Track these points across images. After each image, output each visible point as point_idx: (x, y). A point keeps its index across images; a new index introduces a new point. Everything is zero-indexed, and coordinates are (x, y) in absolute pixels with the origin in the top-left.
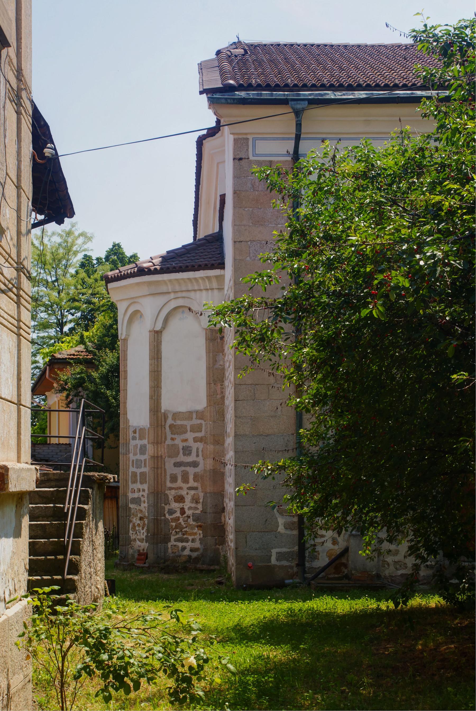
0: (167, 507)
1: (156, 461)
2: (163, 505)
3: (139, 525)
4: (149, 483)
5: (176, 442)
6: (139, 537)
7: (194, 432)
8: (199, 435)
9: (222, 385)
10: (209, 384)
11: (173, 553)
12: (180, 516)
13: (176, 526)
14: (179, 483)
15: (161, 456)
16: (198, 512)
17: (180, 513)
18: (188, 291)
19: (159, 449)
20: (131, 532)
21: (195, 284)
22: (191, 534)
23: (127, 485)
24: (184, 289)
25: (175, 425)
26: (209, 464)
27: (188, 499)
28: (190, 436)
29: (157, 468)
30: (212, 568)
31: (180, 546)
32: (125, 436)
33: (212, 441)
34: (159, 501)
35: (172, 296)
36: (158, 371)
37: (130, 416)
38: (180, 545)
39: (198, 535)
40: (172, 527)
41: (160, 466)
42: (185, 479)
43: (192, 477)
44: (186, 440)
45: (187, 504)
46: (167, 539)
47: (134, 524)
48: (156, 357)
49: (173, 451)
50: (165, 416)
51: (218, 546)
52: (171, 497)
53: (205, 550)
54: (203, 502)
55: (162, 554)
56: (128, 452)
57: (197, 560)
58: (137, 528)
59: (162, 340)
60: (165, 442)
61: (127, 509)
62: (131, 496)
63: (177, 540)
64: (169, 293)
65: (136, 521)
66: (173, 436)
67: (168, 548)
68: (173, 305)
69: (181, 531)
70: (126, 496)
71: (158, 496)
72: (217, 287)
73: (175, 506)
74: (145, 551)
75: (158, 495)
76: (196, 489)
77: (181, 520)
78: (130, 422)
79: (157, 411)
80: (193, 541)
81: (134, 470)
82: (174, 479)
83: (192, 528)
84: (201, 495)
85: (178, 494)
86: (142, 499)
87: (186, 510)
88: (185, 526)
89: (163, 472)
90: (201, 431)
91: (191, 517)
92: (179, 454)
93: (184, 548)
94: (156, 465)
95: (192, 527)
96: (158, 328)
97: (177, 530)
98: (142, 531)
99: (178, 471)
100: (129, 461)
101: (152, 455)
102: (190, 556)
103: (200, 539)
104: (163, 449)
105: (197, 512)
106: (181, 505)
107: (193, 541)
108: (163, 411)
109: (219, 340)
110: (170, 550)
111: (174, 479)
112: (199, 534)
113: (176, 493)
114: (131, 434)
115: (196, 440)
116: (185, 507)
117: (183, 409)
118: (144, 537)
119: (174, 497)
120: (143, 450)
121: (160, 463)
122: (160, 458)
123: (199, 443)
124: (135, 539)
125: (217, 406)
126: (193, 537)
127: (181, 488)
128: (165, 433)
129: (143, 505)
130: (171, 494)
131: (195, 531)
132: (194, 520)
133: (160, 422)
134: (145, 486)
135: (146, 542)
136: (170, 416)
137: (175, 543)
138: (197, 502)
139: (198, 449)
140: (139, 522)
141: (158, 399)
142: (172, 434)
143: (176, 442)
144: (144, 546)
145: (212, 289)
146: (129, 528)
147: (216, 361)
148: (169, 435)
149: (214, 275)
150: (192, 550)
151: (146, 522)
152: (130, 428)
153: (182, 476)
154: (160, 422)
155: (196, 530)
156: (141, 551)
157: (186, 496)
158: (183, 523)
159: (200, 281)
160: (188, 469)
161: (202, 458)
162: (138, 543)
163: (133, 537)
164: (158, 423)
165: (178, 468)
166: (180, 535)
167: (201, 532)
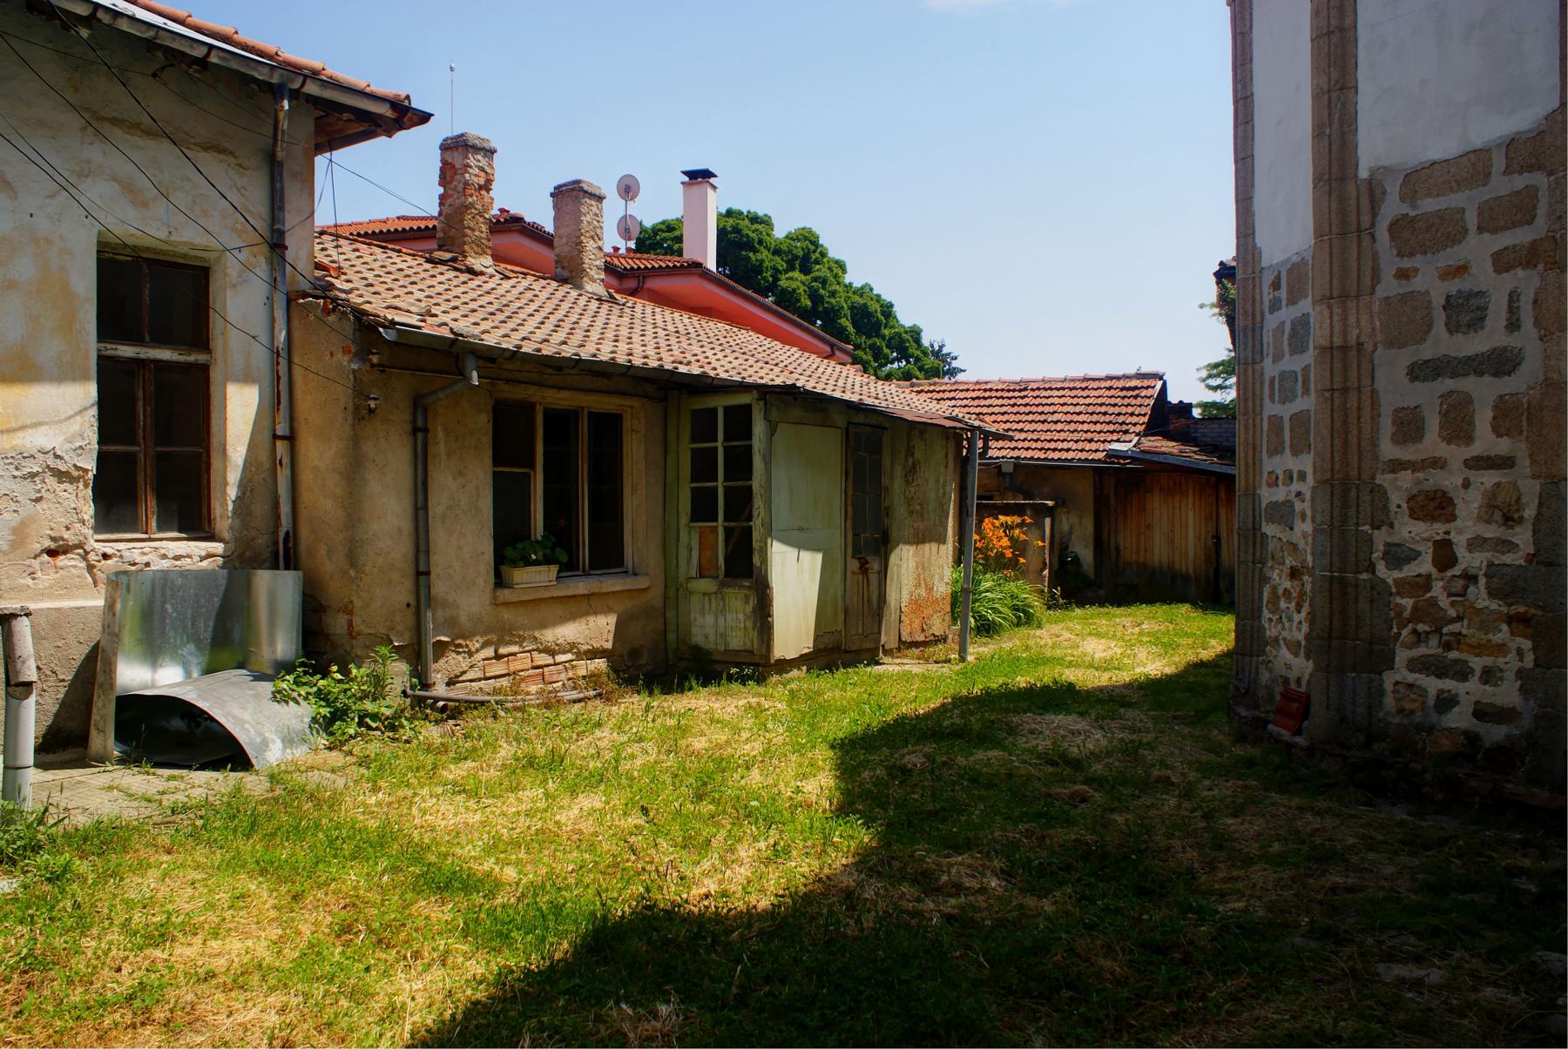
0: (1381, 538)
1: (1338, 365)
2: (1366, 528)
5: (1418, 283)
7: (1494, 231)
8: (1519, 237)
11: (1401, 711)
12: (1434, 571)
13: (1415, 608)
14: (1432, 442)
15: (1360, 344)
16: (1515, 559)
17: (1435, 563)
19: (1352, 320)
20: (1266, 614)
22: (1478, 649)
23: (1256, 463)
25: (1413, 220)
27: (1469, 506)
28: (1478, 249)
29: (1345, 391)
31: (1432, 692)
32: (1249, 307)
34: (1352, 511)
36: (1342, 30)
38: (1432, 685)
39: (1512, 656)
40: (1399, 615)
41: (1353, 383)
42: (1458, 426)
43: (1489, 414)
45: (1466, 526)
47: (1274, 588)
49: (1407, 320)
50: (1374, 191)
52: (1396, 499)
58: (1283, 605)
60: (1373, 292)
61: (1254, 536)
62: (1267, 495)
63: (1415, 665)
65: (1279, 578)
66: (1406, 263)
67: (1382, 693)
69: (1438, 631)
70: (1254, 497)
71: (1349, 495)
73: (1413, 531)
74: (1303, 689)
77: (1437, 590)
78: (1264, 255)
79: (1342, 179)
80: (1489, 675)
82: (1409, 426)
83: (1485, 627)
84: (1530, 489)
85: (1427, 487)
86: (1298, 506)
87: (1461, 552)
88: (1452, 613)
89: (1367, 404)
91: (1482, 581)
92: (1430, 327)
93: (1446, 702)
94: (1337, 379)
95: (1487, 622)
97: (1421, 627)
98: (1297, 617)
99: (1426, 397)
100: (1375, 416)
101: (1326, 343)
102: (1472, 738)
103: (1520, 673)
104: (1364, 318)
105: (1507, 559)
106: (1438, 529)
107: (1489, 675)
108: (1363, 174)
110: (1389, 702)
113: (1418, 482)
114: (1267, 295)
115: (1503, 262)
116: (1453, 537)
117: (1443, 147)
118: (1301, 637)
119: (1411, 499)
120: (1300, 329)
121: (1353, 373)
122: (1353, 353)
123: (1520, 272)
124: (1276, 640)
126: (1488, 661)
127: (1437, 463)
128: (1375, 256)
131: (1498, 638)
132: (1492, 594)
133: (1353, 219)
134: (1306, 463)
135: (1307, 658)
136: (1393, 189)
137: (1411, 677)
138: (1509, 520)
139: (1514, 298)
140: (1288, 584)
141: (1343, 135)
142: (1400, 254)
143: (1418, 283)
146: (1261, 599)
148: (1389, 261)
150: (1482, 712)
151: (1308, 587)
153: (1444, 415)
154: (1353, 219)
155: (1503, 634)
156: (1293, 686)
157: (1458, 496)
158: (1444, 602)
160: (1468, 384)
161: (1534, 333)
162: (1285, 654)
163: (1271, 632)
165: (1428, 384)
166: (1431, 648)
167: (1527, 644)
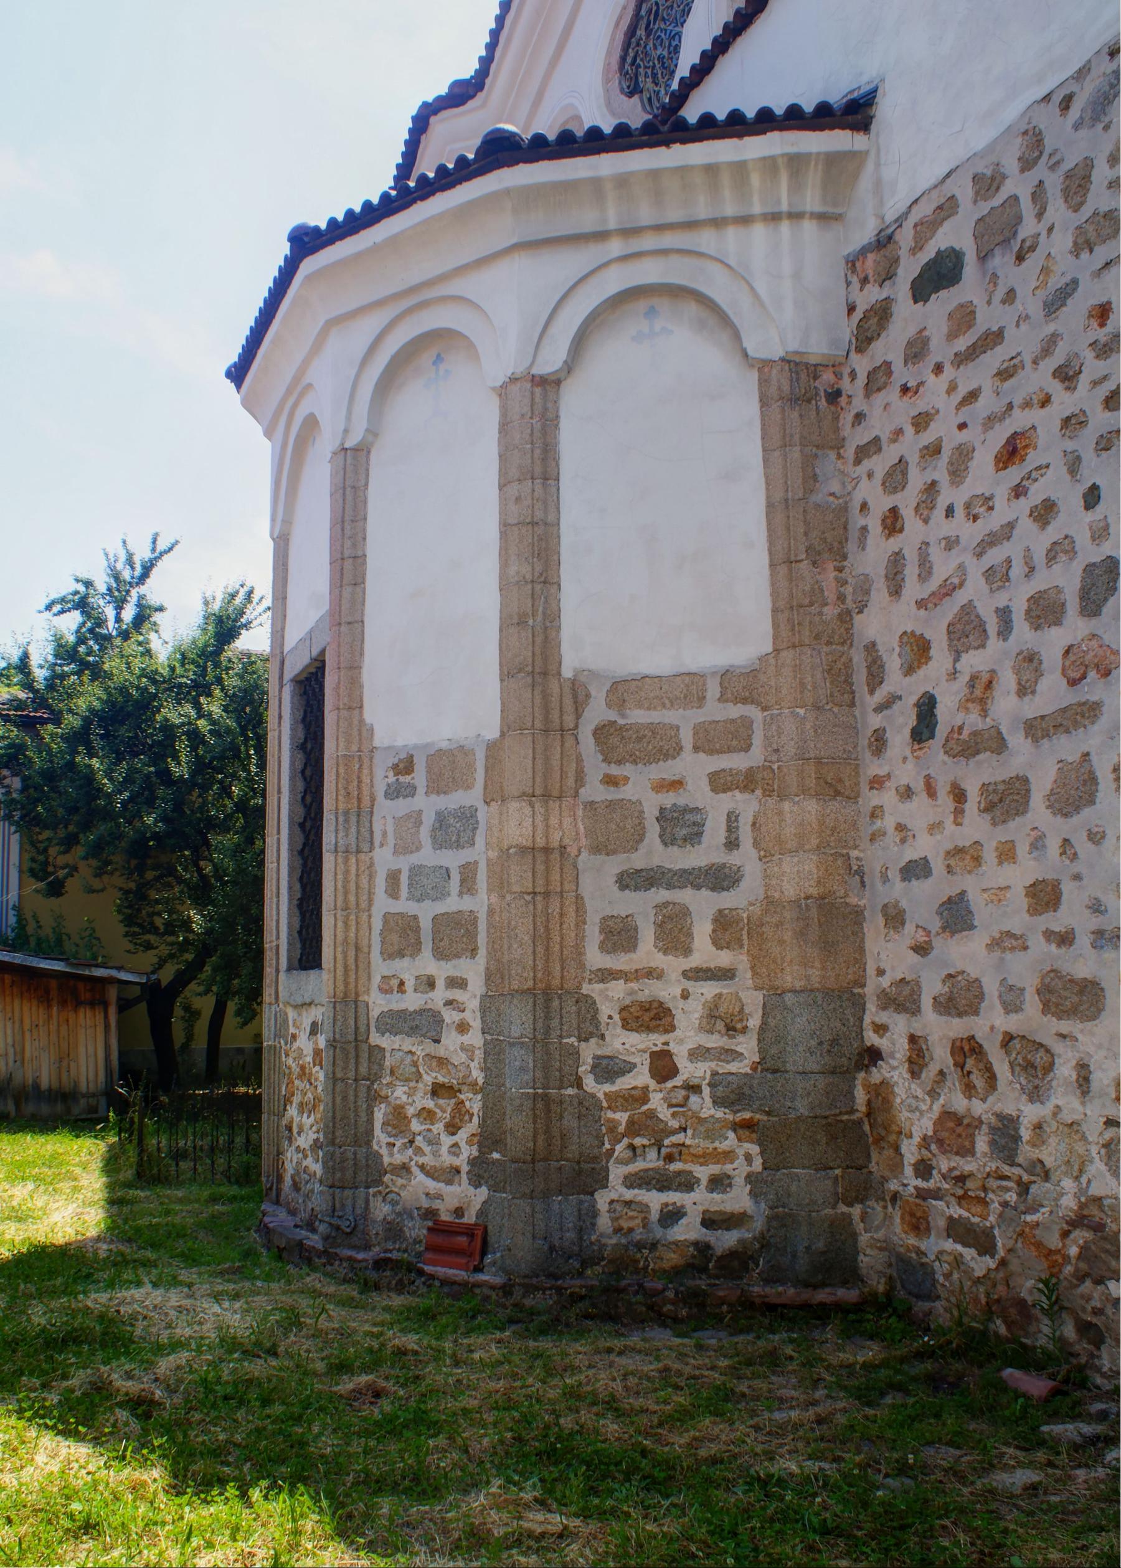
0: (589, 1051)
1: (540, 867)
2: (572, 1040)
3: (427, 1115)
4: (492, 953)
5: (628, 792)
6: (427, 1160)
7: (711, 752)
8: (737, 762)
9: (840, 570)
10: (782, 562)
11: (618, 1230)
12: (653, 1084)
13: (631, 1122)
14: (647, 951)
18: (691, 225)
19: (554, 821)
21: (727, 193)
22: (704, 1158)
24: (674, 215)
26: (797, 875)
30: (822, 1296)
33: (811, 782)
35: (615, 247)
37: (375, 712)
38: (655, 1200)
39: (740, 1161)
40: (612, 1129)
43: (709, 927)
44: (677, 784)
45: (686, 1036)
46: (588, 1176)
48: (538, 470)
49: (615, 829)
51: (843, 1208)
52: (606, 1010)
53: (779, 1220)
54: (763, 1028)
55: (570, 1235)
56: (365, 842)
57: (737, 1262)
59: (562, 414)
60: (576, 795)
63: (631, 1182)
64: (601, 236)
66: (614, 770)
68: (614, 281)
72: (818, 208)
73: (627, 1043)
75: (548, 1001)
76: (725, 974)
77: (656, 1101)
80: (718, 1183)
81: (404, 906)
82: (620, 935)
84: (753, 1001)
85: (642, 997)
86: (450, 1016)
89: (571, 910)
90: (747, 748)
91: (706, 1091)
93: (671, 1216)
94: (540, 882)
96: (551, 360)
97: (638, 1141)
99: (641, 907)
100: (371, 877)
102: (703, 1248)
103: (749, 1178)
105: (733, 1067)
107: (718, 1183)
108: (567, 673)
109: (823, 403)
110: (604, 1223)
111: (620, 935)
112: (745, 1157)
113: (632, 993)
116: (673, 1047)
117: (657, 662)
121: (556, 876)
122: (556, 856)
125: (825, 649)
128: (579, 760)
129: (451, 1042)
130: (610, 998)
133: (555, 715)
137: (629, 1194)
139: (732, 820)
144: (465, 1198)
145: (795, 216)
146: (370, 1121)
147: (815, 477)
149: (824, 148)
150: (710, 1221)
152: (378, 757)
153: (660, 926)
155: (730, 1140)
157: (678, 1007)
158: (664, 1113)
159: (755, 180)
160: (686, 896)
161: (754, 853)
164: (546, 718)
166: (651, 1161)
167: (754, 1149)
